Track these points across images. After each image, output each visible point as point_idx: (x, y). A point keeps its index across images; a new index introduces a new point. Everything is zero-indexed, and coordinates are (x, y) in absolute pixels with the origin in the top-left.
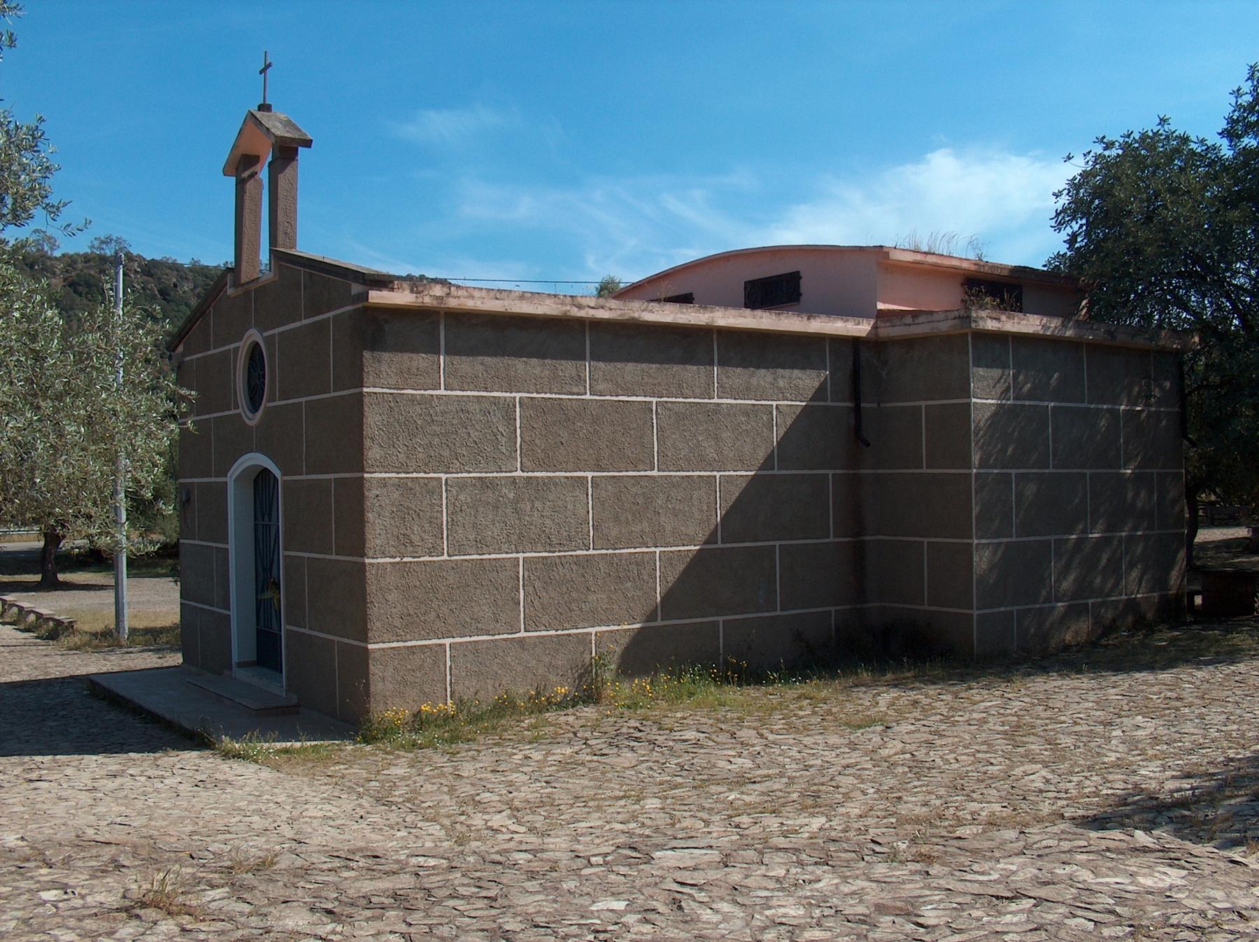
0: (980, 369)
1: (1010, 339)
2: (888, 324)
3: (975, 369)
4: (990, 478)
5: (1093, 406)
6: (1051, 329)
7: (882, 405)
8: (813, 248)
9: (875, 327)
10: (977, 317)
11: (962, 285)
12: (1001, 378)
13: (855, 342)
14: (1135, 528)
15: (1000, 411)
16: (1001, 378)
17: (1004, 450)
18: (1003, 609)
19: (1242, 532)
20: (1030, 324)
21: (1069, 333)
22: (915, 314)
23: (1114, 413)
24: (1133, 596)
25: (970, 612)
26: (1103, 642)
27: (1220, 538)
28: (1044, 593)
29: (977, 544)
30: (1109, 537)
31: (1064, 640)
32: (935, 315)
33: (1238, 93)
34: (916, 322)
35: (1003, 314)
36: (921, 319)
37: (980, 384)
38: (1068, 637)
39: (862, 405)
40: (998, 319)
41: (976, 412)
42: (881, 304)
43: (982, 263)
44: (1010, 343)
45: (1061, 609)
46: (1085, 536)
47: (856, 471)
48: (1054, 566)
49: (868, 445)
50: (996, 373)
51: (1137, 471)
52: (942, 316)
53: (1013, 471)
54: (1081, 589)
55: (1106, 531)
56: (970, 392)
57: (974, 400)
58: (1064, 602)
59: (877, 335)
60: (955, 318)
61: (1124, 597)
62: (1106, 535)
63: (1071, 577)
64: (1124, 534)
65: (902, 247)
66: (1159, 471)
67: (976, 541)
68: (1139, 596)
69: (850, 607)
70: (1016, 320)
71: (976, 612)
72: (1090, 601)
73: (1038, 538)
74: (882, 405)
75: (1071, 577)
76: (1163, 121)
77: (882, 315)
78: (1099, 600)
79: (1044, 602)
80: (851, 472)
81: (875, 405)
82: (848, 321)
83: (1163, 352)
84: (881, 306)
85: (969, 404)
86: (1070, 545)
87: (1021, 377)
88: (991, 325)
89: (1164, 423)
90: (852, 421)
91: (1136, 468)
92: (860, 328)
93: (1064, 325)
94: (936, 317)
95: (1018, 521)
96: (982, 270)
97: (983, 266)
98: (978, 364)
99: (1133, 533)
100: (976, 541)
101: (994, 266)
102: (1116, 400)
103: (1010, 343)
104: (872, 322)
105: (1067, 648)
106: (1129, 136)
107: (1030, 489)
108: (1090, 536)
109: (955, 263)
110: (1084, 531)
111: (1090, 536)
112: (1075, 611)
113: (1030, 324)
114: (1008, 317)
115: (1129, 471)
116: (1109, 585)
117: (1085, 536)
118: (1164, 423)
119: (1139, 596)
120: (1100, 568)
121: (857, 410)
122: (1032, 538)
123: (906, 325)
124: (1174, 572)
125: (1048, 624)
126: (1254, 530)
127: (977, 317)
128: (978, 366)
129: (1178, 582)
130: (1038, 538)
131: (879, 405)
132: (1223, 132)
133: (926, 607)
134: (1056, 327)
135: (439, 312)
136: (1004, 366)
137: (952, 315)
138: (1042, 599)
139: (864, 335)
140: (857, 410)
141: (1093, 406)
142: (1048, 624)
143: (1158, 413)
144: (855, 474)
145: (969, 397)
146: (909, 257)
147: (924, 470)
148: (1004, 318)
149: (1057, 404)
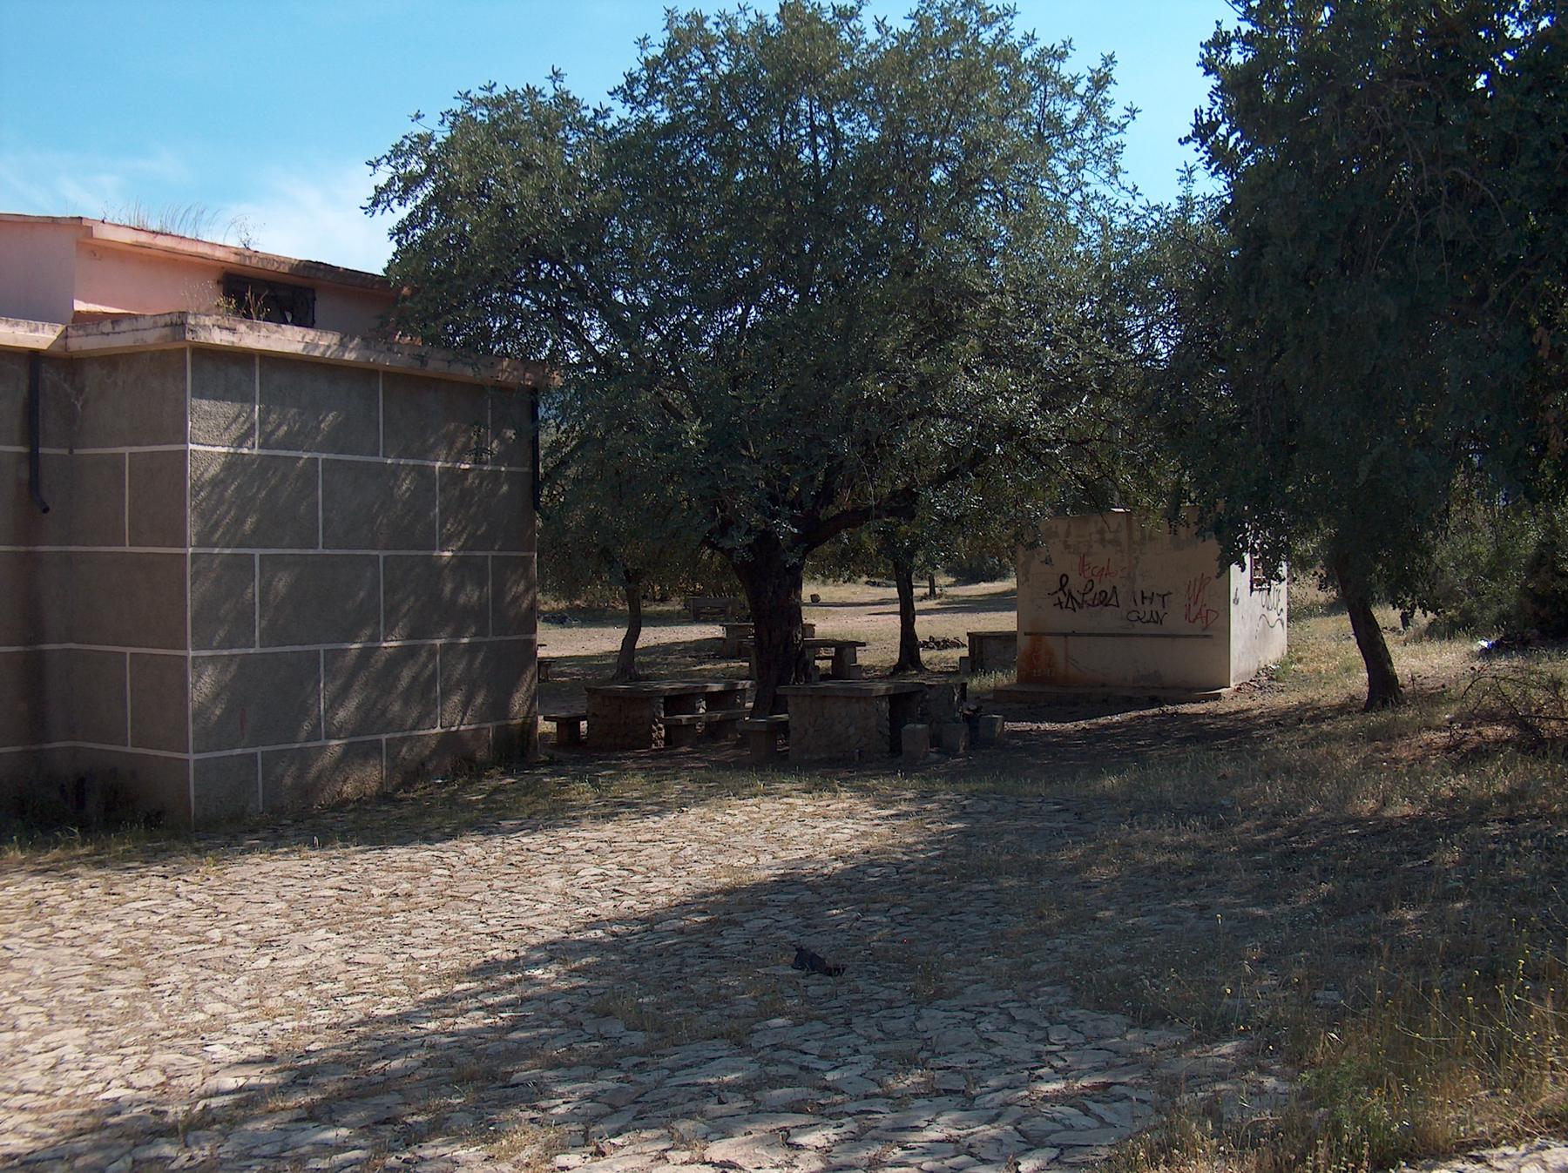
0: (205, 402)
1: (257, 361)
2: (81, 332)
3: (195, 402)
4: (217, 561)
5: (389, 461)
6: (322, 349)
7: (76, 451)
8: (21, 219)
9: (64, 336)
10: (197, 325)
11: (218, 282)
12: (238, 416)
13: (33, 357)
14: (458, 633)
15: (233, 464)
16: (238, 416)
17: (239, 521)
18: (238, 751)
19: (715, 631)
20: (288, 339)
21: (350, 356)
22: (115, 319)
23: (424, 473)
24: (453, 729)
25: (184, 756)
26: (401, 794)
27: (700, 637)
28: (306, 726)
29: (194, 658)
30: (415, 646)
31: (339, 794)
32: (141, 320)
33: (643, 43)
34: (117, 329)
35: (241, 322)
36: (124, 326)
37: (203, 424)
38: (348, 789)
39: (41, 450)
40: (233, 330)
41: (195, 464)
42: (81, 303)
43: (247, 253)
44: (257, 367)
45: (337, 749)
46: (377, 645)
47: (30, 548)
48: (325, 690)
49: (46, 510)
50: (228, 408)
51: (461, 553)
52: (148, 323)
53: (257, 552)
54: (370, 718)
55: (410, 637)
56: (186, 434)
57: (191, 446)
58: (339, 739)
59: (66, 348)
60: (166, 326)
61: (438, 729)
62: (407, 643)
63: (352, 704)
64: (438, 642)
65: (117, 222)
66: (494, 553)
67: (191, 653)
68: (462, 728)
69: (19, 749)
70: (264, 332)
71: (192, 757)
72: (384, 737)
73: (297, 648)
74: (76, 451)
75: (352, 704)
76: (556, 76)
77: (81, 319)
78: (399, 735)
79: (307, 741)
80: (22, 549)
81: (65, 452)
82: (17, 324)
83: (502, 389)
84: (80, 306)
85: (185, 452)
86: (349, 660)
87: (273, 417)
88: (220, 338)
89: (505, 488)
90: (25, 475)
91: (460, 549)
92: (42, 337)
93: (342, 345)
94: (141, 324)
95: (264, 623)
96: (248, 262)
97: (250, 257)
98: (200, 394)
99: (454, 640)
100: (191, 653)
101: (268, 258)
102: (424, 453)
103: (257, 367)
104: (60, 328)
105: (341, 805)
106: (490, 89)
107: (282, 583)
108: (385, 645)
109: (202, 249)
110: (374, 638)
111: (385, 645)
112: (357, 753)
113: (288, 339)
114: (251, 328)
115: (449, 554)
116: (415, 714)
117: (377, 645)
118: (505, 488)
119: (462, 728)
120: (400, 688)
121: (33, 459)
122: (287, 649)
123: (103, 333)
124: (518, 695)
125: (314, 771)
126: (729, 630)
127: (197, 325)
128: (201, 398)
129: (526, 708)
130: (297, 648)
131: (71, 452)
132: (616, 91)
133: (129, 749)
134: (329, 347)
135: (377, 371)
136: (246, 398)
137: (162, 321)
138: (303, 735)
139: (45, 347)
140: (33, 459)
141: (389, 461)
142: (314, 771)
143: (496, 475)
144: (28, 553)
145: (185, 442)
146: (127, 237)
147: (127, 549)
148: (242, 328)
149: (332, 456)
